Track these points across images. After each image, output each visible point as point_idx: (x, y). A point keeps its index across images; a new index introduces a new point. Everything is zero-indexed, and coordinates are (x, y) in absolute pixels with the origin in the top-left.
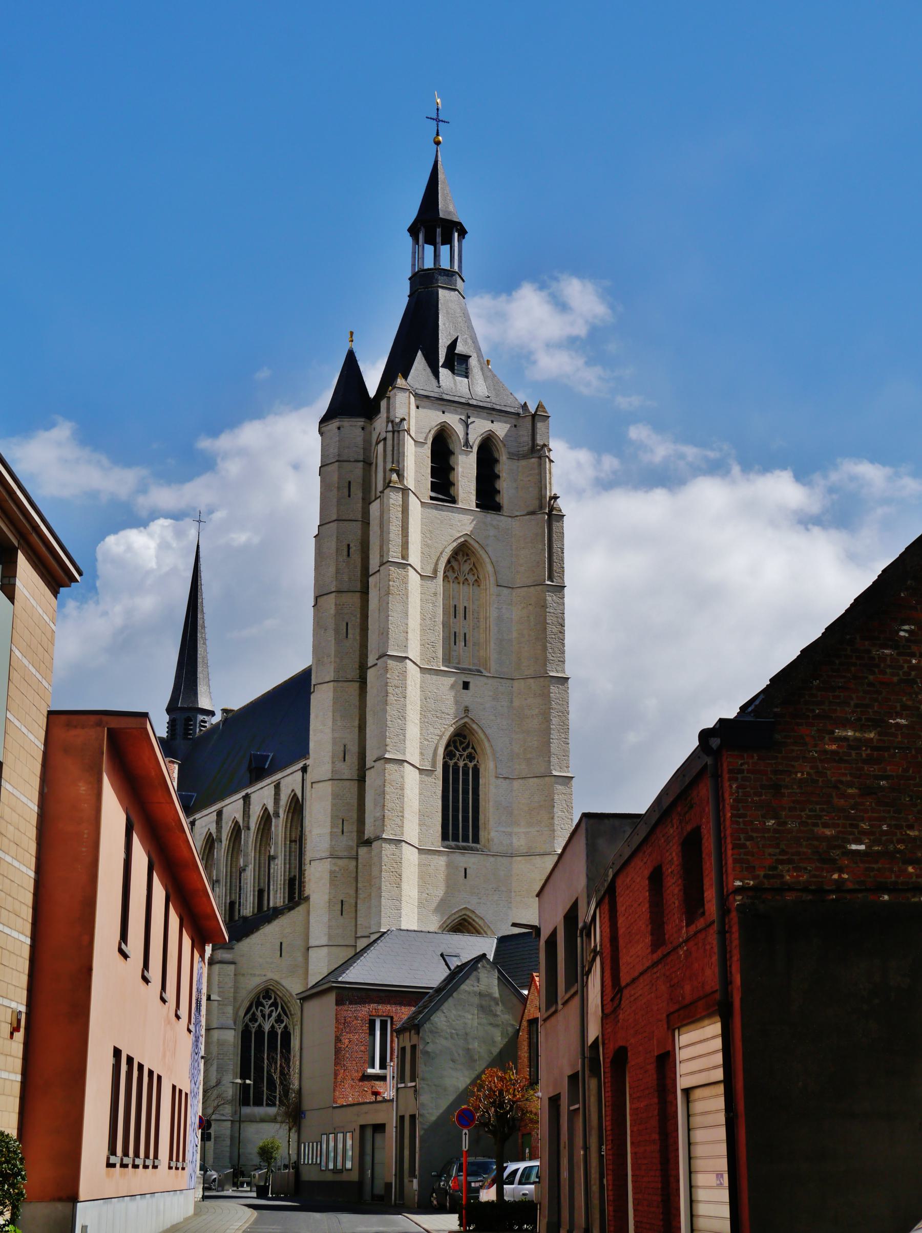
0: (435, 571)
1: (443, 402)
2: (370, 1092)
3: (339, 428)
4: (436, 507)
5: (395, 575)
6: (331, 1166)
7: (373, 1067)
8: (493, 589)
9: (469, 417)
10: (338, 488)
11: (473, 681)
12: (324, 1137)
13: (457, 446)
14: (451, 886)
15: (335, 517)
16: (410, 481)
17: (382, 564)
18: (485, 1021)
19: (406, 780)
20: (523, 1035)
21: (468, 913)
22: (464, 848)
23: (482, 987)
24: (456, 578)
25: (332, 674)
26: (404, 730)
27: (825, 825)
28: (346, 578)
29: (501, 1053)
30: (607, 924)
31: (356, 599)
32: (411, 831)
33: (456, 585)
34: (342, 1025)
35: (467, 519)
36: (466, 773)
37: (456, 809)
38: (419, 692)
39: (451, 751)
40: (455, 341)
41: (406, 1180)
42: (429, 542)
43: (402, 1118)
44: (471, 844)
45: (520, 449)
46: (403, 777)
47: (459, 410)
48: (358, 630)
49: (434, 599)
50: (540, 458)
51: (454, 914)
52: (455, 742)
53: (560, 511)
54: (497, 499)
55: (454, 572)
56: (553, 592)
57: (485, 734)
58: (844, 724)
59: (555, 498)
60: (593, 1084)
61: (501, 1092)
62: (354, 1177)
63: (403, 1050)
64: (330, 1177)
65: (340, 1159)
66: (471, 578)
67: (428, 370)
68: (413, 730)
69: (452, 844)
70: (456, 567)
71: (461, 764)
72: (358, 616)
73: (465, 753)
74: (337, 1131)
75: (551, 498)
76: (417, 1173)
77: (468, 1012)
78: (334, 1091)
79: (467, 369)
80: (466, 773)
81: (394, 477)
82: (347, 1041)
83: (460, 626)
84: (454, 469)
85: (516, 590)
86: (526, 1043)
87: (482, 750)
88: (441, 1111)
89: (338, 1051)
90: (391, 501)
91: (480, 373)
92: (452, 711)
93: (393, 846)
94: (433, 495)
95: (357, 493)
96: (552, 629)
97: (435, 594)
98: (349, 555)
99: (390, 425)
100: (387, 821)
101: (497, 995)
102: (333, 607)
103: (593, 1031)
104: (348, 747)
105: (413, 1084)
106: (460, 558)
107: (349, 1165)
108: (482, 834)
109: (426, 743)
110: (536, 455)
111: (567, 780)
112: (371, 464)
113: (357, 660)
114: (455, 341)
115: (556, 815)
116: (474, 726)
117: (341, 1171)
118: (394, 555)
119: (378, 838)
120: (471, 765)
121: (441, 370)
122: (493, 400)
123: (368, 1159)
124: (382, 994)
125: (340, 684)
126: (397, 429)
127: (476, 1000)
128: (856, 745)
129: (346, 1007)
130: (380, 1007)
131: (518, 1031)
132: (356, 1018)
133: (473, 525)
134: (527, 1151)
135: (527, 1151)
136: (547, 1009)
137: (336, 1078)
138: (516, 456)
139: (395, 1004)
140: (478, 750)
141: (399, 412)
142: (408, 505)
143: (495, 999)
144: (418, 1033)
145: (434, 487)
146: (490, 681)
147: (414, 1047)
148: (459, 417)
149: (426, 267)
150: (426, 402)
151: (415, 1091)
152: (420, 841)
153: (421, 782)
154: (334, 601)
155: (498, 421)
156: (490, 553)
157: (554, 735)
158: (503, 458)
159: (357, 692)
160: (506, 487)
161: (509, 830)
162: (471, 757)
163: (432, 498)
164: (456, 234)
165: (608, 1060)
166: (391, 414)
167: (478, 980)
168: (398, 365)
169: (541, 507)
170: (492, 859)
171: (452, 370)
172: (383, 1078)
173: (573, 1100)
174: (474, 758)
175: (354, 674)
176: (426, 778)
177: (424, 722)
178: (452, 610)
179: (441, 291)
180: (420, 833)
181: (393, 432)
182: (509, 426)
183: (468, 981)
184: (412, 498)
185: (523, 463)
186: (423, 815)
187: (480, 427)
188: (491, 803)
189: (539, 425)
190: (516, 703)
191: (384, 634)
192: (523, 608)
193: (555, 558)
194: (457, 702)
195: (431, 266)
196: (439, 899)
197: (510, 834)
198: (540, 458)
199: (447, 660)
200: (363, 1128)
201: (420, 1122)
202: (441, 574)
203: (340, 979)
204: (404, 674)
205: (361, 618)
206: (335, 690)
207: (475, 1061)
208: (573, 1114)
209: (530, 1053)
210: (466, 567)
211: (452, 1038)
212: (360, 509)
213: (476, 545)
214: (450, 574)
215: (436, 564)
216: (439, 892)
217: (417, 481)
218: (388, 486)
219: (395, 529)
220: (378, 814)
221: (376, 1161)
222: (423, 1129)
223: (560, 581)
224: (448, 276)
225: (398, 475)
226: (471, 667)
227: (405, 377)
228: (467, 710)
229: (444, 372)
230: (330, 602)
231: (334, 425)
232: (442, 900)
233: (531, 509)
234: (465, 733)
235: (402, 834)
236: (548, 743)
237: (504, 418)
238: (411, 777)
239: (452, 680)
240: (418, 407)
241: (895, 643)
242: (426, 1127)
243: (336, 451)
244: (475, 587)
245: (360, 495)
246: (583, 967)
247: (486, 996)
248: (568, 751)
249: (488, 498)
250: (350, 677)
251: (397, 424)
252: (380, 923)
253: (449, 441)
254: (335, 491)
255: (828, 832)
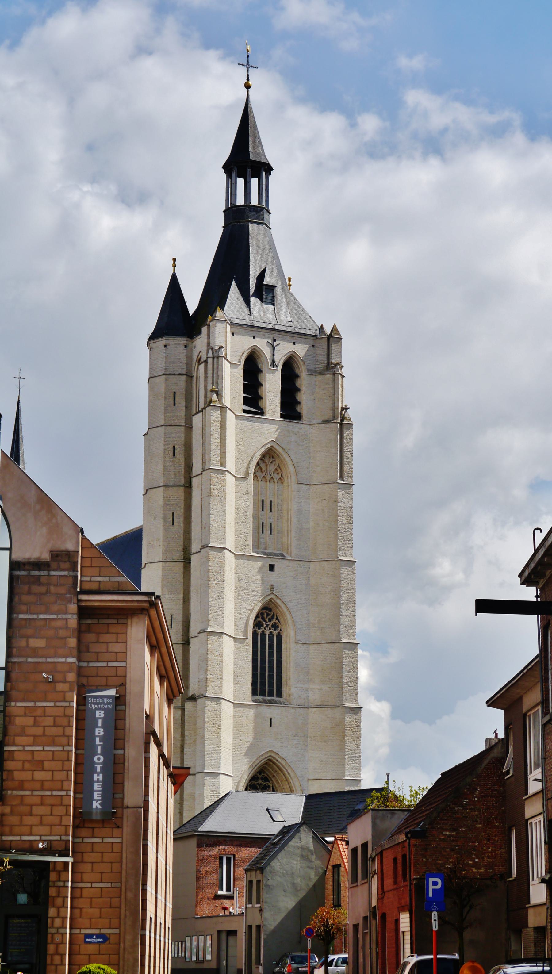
0: (247, 473)
1: (253, 329)
2: (220, 907)
3: (165, 346)
4: (248, 419)
5: (215, 480)
6: (194, 958)
7: (222, 890)
8: (294, 486)
9: (275, 340)
10: (165, 397)
11: (277, 564)
12: (188, 939)
13: (265, 365)
14: (258, 733)
15: (162, 423)
16: (227, 401)
17: (204, 470)
18: (304, 865)
19: (224, 649)
20: (329, 874)
21: (273, 755)
22: (270, 702)
23: (303, 843)
24: (264, 477)
25: (161, 556)
26: (222, 608)
27: (440, 860)
28: (172, 474)
29: (314, 886)
30: (379, 864)
31: (180, 492)
32: (228, 690)
33: (263, 483)
34: (201, 861)
35: (273, 428)
36: (271, 640)
37: (263, 669)
38: (234, 575)
39: (260, 622)
40: (263, 272)
41: (254, 967)
42: (242, 448)
43: (250, 927)
44: (275, 698)
45: (318, 366)
46: (221, 647)
47: (267, 334)
48: (182, 519)
49: (246, 497)
50: (334, 374)
51: (262, 756)
52: (262, 614)
53: (350, 420)
54: (298, 409)
55: (262, 472)
56: (343, 489)
57: (287, 608)
58: (446, 830)
59: (346, 409)
60: (373, 922)
61: (327, 920)
62: (214, 965)
63: (251, 882)
64: (193, 966)
65: (201, 953)
66: (276, 477)
67: (241, 298)
68: (230, 606)
69: (260, 698)
70: (264, 468)
71: (267, 632)
72: (182, 507)
73: (271, 623)
74: (199, 934)
75: (343, 409)
76: (262, 962)
77: (294, 859)
78: (196, 906)
79: (273, 297)
80: (271, 640)
81: (214, 397)
82: (204, 872)
83: (267, 517)
84: (262, 385)
85: (311, 486)
86: (331, 880)
87: (285, 620)
88: (277, 923)
89: (198, 879)
90: (212, 418)
91: (284, 300)
92: (259, 590)
93: (214, 703)
94: (246, 408)
95: (181, 402)
96: (343, 520)
97: (247, 492)
98: (174, 455)
99: (210, 351)
100: (209, 683)
101: (312, 848)
102: (162, 499)
103: (374, 903)
104: (174, 617)
105: (259, 905)
106: (266, 460)
107: (209, 957)
108: (284, 689)
109: (239, 616)
110: (330, 372)
111: (353, 646)
112: (192, 377)
113: (181, 543)
114: (263, 272)
115: (344, 675)
116: (278, 601)
117: (202, 962)
118: (215, 464)
119: (202, 696)
120: (275, 633)
121: (252, 299)
122: (295, 324)
123: (223, 953)
124: (228, 839)
125: (168, 564)
126: (216, 355)
127: (299, 852)
128: (449, 836)
129: (203, 849)
130: (226, 848)
131: (326, 871)
132: (211, 856)
133: (277, 433)
134: (331, 948)
135: (331, 948)
136: (352, 883)
137: (197, 898)
138: (313, 372)
139: (237, 846)
140: (281, 620)
141: (218, 342)
142: (226, 421)
143: (310, 851)
144: (262, 873)
145: (246, 401)
146: (291, 563)
147: (259, 882)
148: (266, 341)
149: (238, 204)
150: (240, 329)
151: (261, 910)
152: (234, 697)
153: (236, 648)
154: (162, 494)
155: (299, 343)
156: (292, 456)
157: (344, 609)
158: (303, 373)
159: (182, 570)
160: (305, 398)
161: (306, 686)
162: (275, 627)
163: (245, 411)
164: (264, 173)
165: (380, 916)
166: (211, 341)
167: (300, 839)
168: (214, 296)
169: (334, 417)
170: (292, 710)
171: (261, 299)
172: (231, 898)
173: (365, 927)
174: (278, 627)
175: (179, 555)
176: (239, 645)
177: (238, 599)
178: (261, 504)
179: (251, 226)
180: (235, 691)
181: (213, 358)
182: (308, 346)
183: (293, 840)
184: (229, 414)
185: (320, 378)
186: (237, 675)
187: (284, 349)
188: (292, 665)
189: (333, 346)
190: (313, 581)
191: (206, 527)
192: (319, 502)
193: (345, 460)
194: (263, 582)
195: (242, 203)
196: (249, 743)
197: (307, 690)
198: (334, 374)
199: (256, 547)
200: (219, 932)
201: (264, 931)
202: (251, 475)
203: (199, 829)
204: (222, 562)
205: (185, 509)
206: (163, 570)
207: (298, 891)
208: (365, 934)
209: (333, 886)
210: (272, 468)
211: (284, 876)
212: (183, 416)
213: (280, 450)
214: (259, 474)
215: (248, 467)
216: (249, 739)
217: (233, 398)
218: (209, 405)
219: (215, 440)
220: (202, 677)
221: (229, 955)
222: (266, 934)
223: (349, 479)
224: (257, 211)
225: (217, 395)
226: (275, 552)
227: (222, 308)
228: (272, 588)
229: (254, 301)
230: (159, 495)
231: (162, 342)
232: (251, 744)
233: (326, 418)
234: (271, 607)
235: (221, 692)
236: (339, 616)
237: (304, 340)
238: (228, 644)
239: (259, 564)
240: (233, 334)
241: (462, 805)
242: (267, 933)
243: (163, 365)
244: (279, 484)
245: (183, 404)
246: (370, 874)
247: (305, 849)
248: (355, 622)
249: (290, 410)
250: (176, 558)
251: (216, 351)
252: (204, 765)
253: (258, 361)
254: (162, 401)
255: (440, 862)
